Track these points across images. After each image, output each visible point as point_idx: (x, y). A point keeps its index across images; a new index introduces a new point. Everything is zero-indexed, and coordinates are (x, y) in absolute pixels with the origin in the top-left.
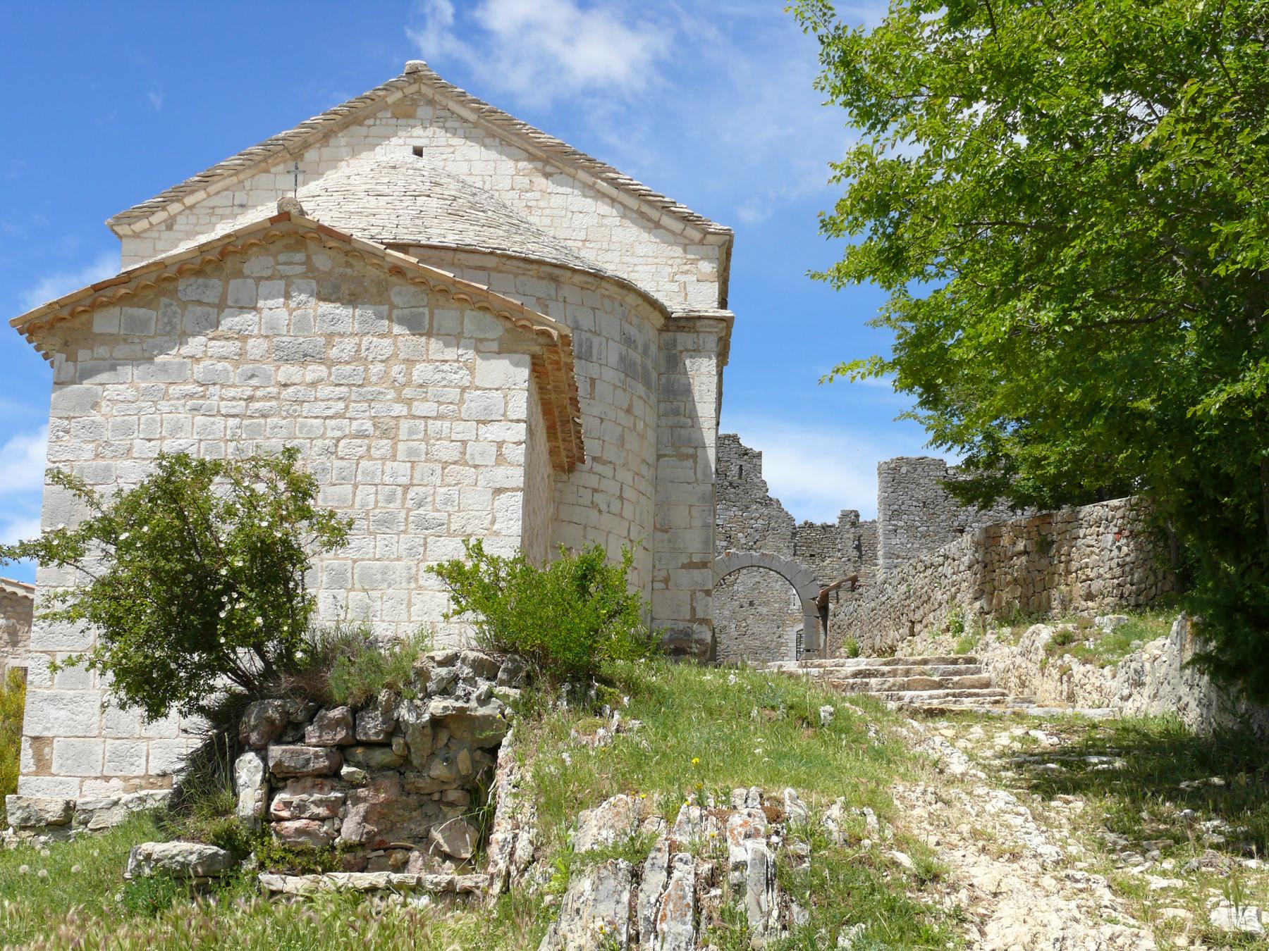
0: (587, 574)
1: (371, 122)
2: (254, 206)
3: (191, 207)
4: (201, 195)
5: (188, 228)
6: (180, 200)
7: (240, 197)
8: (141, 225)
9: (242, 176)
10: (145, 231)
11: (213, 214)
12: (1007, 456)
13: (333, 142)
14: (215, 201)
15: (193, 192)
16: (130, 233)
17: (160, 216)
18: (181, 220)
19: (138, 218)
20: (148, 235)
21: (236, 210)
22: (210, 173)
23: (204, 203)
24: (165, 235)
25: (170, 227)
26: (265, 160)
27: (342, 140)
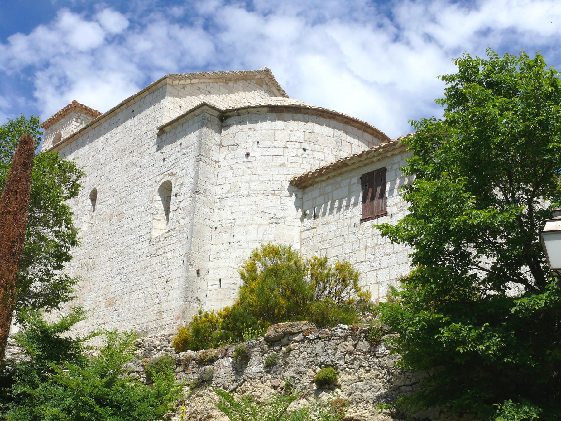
0: (267, 300)
1: (249, 81)
2: (213, 94)
3: (192, 84)
4: (197, 81)
5: (190, 91)
6: (191, 79)
7: (209, 89)
8: (176, 82)
9: (211, 81)
10: (176, 85)
11: (199, 90)
12: (118, 416)
13: (237, 82)
14: (200, 85)
15: (195, 78)
16: (171, 83)
17: (182, 82)
18: (188, 87)
19: (177, 79)
20: (176, 87)
21: (207, 92)
22: (203, 74)
23: (196, 85)
24: (182, 90)
25: (184, 88)
26: (219, 78)
27: (240, 83)
